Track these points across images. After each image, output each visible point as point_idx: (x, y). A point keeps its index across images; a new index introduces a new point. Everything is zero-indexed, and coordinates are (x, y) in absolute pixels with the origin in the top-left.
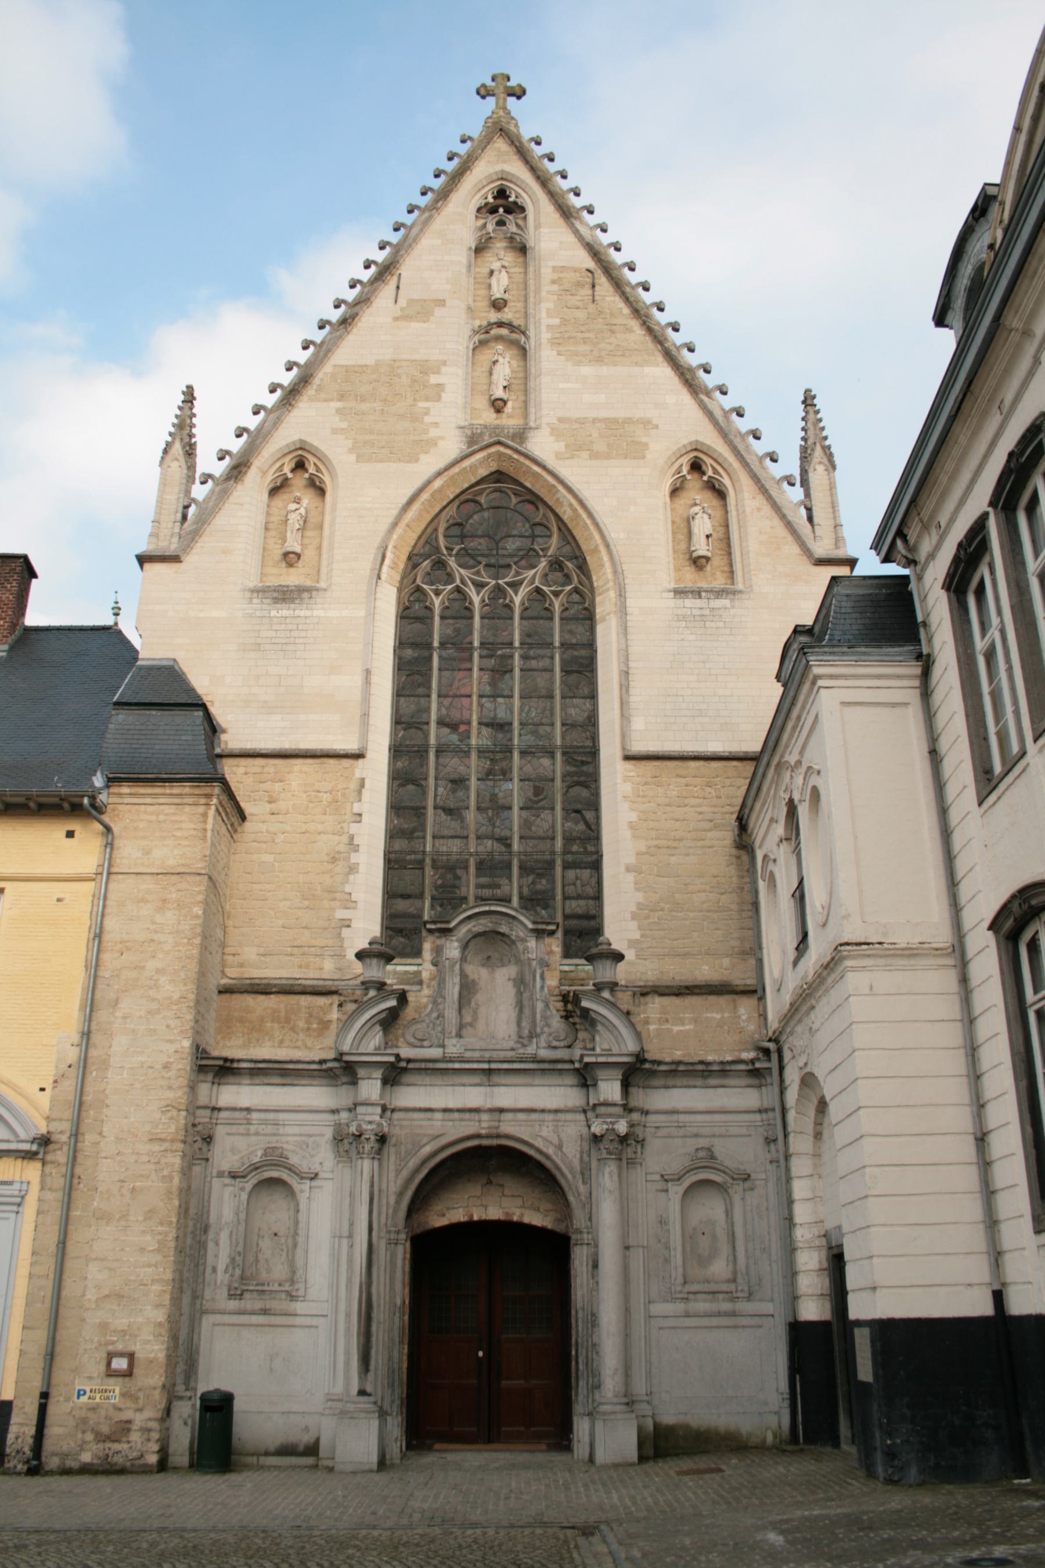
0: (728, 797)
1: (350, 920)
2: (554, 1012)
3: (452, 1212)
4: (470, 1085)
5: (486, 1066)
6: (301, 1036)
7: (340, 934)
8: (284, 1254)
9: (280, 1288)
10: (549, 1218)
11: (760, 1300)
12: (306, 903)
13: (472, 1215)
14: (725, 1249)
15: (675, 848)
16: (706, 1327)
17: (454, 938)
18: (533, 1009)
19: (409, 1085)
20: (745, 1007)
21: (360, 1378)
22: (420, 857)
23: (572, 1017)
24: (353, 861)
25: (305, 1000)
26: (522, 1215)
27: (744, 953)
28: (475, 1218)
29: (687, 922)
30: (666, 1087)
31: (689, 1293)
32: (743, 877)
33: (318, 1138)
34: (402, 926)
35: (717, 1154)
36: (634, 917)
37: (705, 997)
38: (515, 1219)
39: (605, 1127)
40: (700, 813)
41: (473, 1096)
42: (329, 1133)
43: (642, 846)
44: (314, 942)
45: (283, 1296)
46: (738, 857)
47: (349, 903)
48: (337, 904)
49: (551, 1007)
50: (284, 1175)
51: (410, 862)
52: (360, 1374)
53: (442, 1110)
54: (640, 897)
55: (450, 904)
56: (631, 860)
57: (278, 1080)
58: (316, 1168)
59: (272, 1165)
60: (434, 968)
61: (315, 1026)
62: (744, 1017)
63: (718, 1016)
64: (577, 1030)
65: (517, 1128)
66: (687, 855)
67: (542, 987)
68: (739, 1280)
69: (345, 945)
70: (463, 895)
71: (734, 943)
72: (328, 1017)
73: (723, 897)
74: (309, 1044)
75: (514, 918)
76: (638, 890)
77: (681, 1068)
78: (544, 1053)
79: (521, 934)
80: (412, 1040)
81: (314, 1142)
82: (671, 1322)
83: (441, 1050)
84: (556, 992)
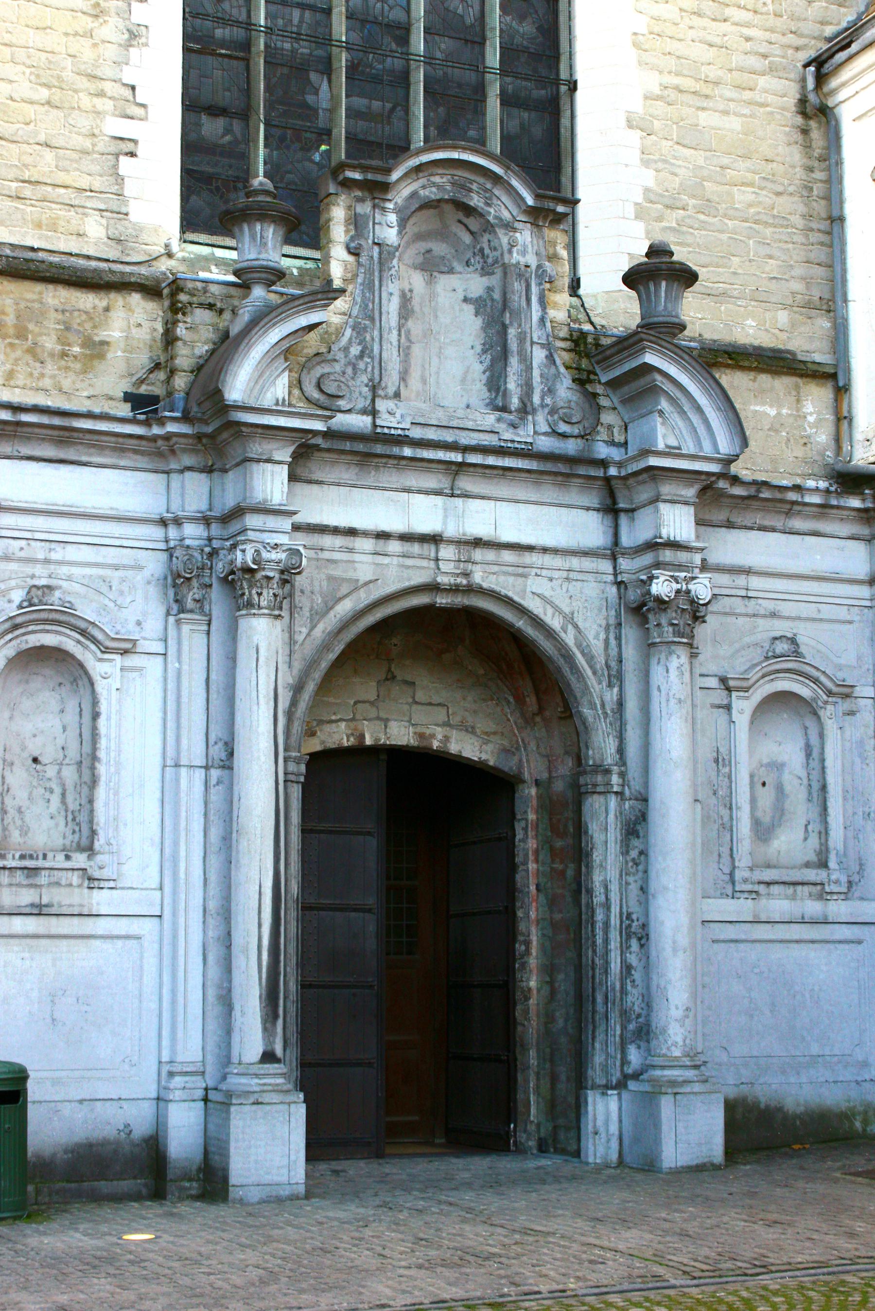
0: (792, 17)
1: (135, 142)
2: (562, 370)
3: (327, 728)
4: (419, 492)
5: (458, 457)
6: (50, 368)
7: (116, 166)
8: (55, 799)
9: (68, 865)
10: (489, 747)
11: (862, 899)
12: (44, 94)
13: (362, 736)
14: (800, 809)
15: (707, 96)
16: (781, 941)
17: (391, 206)
18: (526, 361)
19: (310, 482)
20: (815, 401)
21: (265, 1029)
22: (239, 33)
23: (590, 381)
24: (136, 18)
25: (55, 297)
26: (447, 739)
27: (808, 305)
28: (368, 741)
29: (724, 237)
30: (730, 525)
31: (760, 883)
32: (811, 170)
33: (130, 573)
34: (209, 169)
35: (803, 649)
36: (640, 214)
37: (752, 375)
38: (435, 745)
39: (676, 586)
40: (748, 39)
41: (425, 513)
42: (154, 565)
43: (653, 82)
44: (62, 177)
45: (75, 878)
46: (805, 132)
47: (130, 102)
48: (106, 105)
49: (558, 362)
50: (69, 642)
51: (223, 44)
52: (264, 1022)
53: (377, 534)
54: (648, 178)
55: (299, 139)
56: (638, 107)
57: (50, 451)
58: (130, 631)
59: (46, 621)
60: (351, 259)
61: (76, 349)
62: (811, 419)
63: (773, 412)
64: (599, 408)
65: (502, 578)
66: (726, 113)
67: (542, 320)
68: (832, 864)
69: (126, 193)
70: (321, 125)
71: (798, 286)
72: (102, 335)
73: (781, 200)
74: (66, 384)
75: (496, 179)
76: (646, 163)
77: (765, 494)
78: (545, 444)
79: (506, 215)
80: (316, 395)
81: (123, 580)
82: (731, 932)
83: (368, 420)
84: (564, 333)
